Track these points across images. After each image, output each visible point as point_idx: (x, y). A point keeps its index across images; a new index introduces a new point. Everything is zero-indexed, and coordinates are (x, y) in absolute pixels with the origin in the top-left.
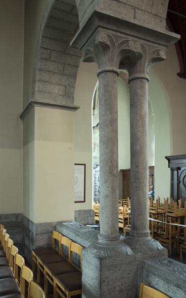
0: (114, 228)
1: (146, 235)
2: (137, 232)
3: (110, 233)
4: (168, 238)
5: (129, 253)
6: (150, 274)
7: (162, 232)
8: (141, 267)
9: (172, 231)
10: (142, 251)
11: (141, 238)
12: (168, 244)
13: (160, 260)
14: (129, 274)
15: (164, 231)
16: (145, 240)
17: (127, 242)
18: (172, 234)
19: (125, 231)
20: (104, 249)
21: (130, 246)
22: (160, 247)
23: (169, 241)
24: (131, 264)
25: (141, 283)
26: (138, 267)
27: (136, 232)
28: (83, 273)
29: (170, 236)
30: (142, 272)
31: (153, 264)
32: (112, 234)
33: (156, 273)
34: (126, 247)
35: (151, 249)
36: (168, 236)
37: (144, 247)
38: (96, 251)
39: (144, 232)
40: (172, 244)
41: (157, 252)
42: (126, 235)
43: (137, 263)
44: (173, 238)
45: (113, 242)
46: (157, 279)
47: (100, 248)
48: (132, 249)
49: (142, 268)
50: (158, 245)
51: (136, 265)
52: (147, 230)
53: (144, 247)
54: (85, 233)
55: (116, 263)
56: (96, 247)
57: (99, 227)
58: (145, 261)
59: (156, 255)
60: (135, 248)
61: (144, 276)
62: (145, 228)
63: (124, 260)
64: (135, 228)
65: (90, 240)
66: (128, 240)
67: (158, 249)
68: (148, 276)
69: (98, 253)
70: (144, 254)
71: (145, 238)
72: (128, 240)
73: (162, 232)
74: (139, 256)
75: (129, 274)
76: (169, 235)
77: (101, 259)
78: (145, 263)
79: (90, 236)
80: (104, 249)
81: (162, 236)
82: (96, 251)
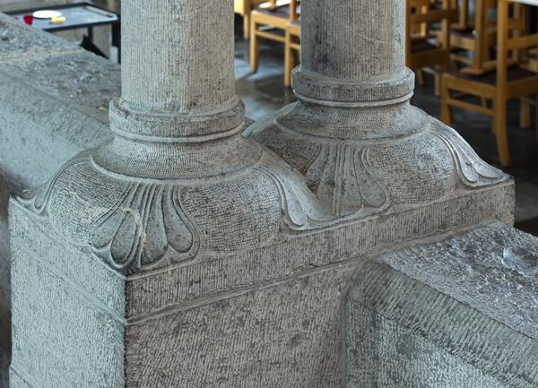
0: (207, 66)
1: (386, 98)
2: (342, 81)
3: (183, 102)
4: (488, 76)
5: (295, 218)
6: (421, 342)
7: (454, 40)
8: (368, 293)
9: (510, 34)
10: (372, 199)
11: (361, 121)
12: (490, 104)
13: (470, 250)
14: (295, 341)
15: (467, 32)
16: (385, 131)
17: (282, 146)
18: (509, 53)
19: (251, 33)
20: (147, 199)
21: (303, 171)
22: (477, 168)
23: (498, 92)
24: (306, 281)
25: (249, 123)
26: (346, 297)
27: (334, 82)
28: (17, 341)
29: (500, 63)
30: (375, 323)
31: (435, 280)
32: (193, 104)
33: (456, 332)
34: (281, 177)
35: (421, 186)
36: (488, 65)
37: (381, 173)
38: (98, 211)
39: (379, 81)
40: (512, 105)
41: (454, 201)
42: (261, 55)
43: (343, 270)
44: (515, 71)
45: (201, 154)
46: (463, 369)
47: (124, 192)
48: (312, 187)
49: (373, 303)
50: (450, 153)
51: (337, 283)
52: (388, 66)
53: (381, 173)
54: (31, 73)
55: (220, 283)
56: (97, 189)
57: (116, 27)
58: (390, 259)
59: (447, 225)
60: (332, 184)
61: (386, 346)
62: (382, 56)
63: (266, 258)
64: (325, 59)
65: (55, 118)
66: (289, 133)
67: (461, 182)
68: (405, 349)
69: (111, 227)
70: (382, 218)
71: (387, 116)
72: (289, 133)
73: (454, 40)
74: (356, 228)
75: (295, 341)
76: (493, 55)
77: (130, 265)
78: (387, 268)
79: (56, 93)
80: (147, 199)
81: (453, 57)
82: (98, 211)
